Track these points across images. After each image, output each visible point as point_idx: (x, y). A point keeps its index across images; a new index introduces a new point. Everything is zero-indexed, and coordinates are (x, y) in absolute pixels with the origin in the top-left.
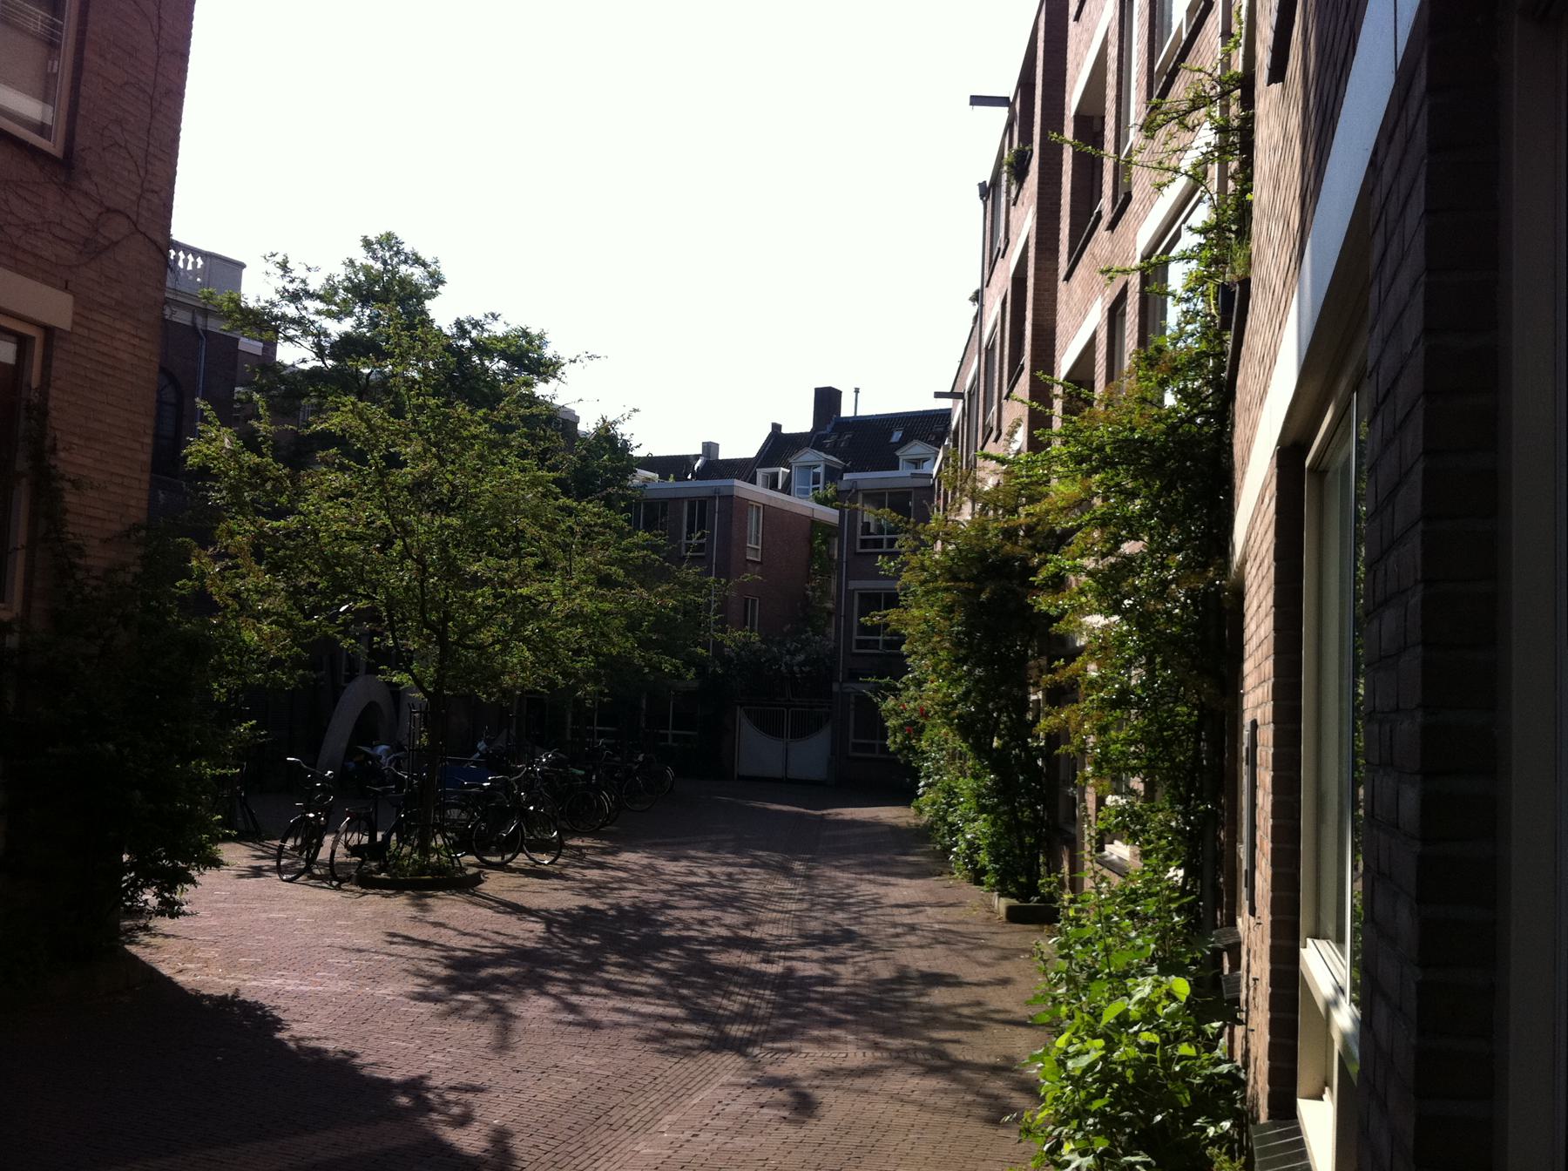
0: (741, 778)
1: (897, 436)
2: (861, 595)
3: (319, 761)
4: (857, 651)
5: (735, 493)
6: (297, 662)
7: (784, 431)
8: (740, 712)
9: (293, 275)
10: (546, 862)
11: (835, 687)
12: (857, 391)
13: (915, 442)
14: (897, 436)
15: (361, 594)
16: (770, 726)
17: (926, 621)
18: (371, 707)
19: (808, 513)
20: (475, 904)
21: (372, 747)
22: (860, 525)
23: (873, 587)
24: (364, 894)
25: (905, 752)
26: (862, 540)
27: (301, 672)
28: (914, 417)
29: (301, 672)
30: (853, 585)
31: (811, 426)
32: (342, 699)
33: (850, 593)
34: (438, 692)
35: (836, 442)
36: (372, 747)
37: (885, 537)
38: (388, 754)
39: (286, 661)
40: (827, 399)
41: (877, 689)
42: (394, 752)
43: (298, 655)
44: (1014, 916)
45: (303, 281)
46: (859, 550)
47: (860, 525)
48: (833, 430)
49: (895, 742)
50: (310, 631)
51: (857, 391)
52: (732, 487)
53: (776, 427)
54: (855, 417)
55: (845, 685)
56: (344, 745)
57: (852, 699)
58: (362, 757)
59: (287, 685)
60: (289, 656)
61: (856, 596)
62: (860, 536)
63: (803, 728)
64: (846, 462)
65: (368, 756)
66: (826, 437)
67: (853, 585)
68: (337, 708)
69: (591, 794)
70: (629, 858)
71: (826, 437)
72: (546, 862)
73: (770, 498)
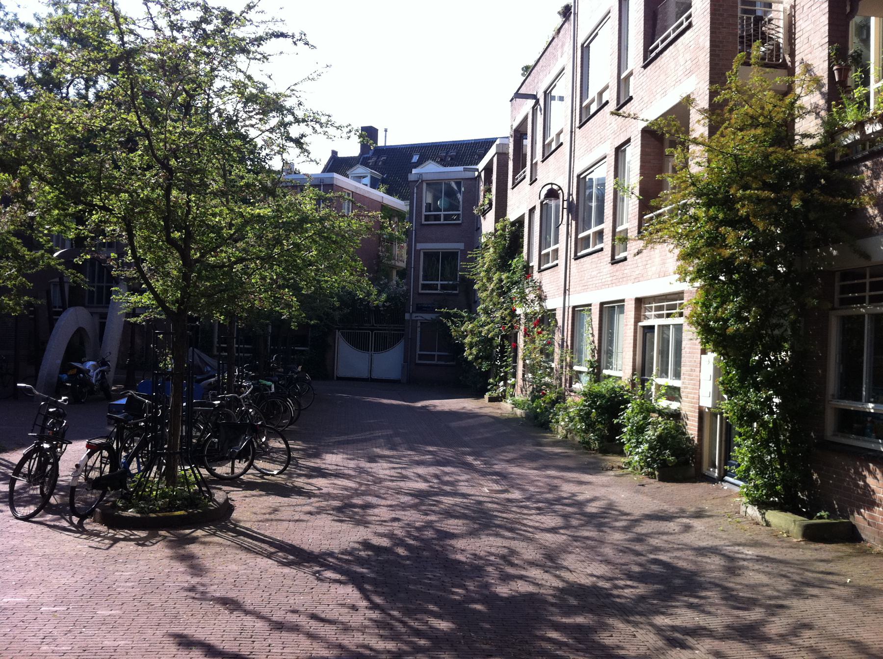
0: (340, 379)
1: (415, 158)
2: (425, 253)
3: (40, 375)
4: (423, 292)
5: (335, 183)
6: (21, 290)
7: (339, 155)
8: (338, 334)
9: (6, 10)
10: (275, 472)
11: (407, 316)
12: (386, 131)
13: (430, 161)
14: (415, 158)
15: (96, 205)
16: (360, 343)
17: (707, 232)
18: (80, 332)
19: (380, 200)
20: (248, 550)
21: (82, 363)
22: (424, 205)
23: (441, 247)
24: (115, 541)
25: (480, 361)
26: (425, 215)
27: (26, 298)
28: (429, 147)
29: (26, 298)
30: (420, 246)
31: (359, 151)
32: (56, 325)
33: (418, 252)
34: (181, 312)
35: (376, 162)
36: (82, 363)
37: (442, 213)
38: (95, 368)
39: (12, 289)
40: (369, 133)
41: (448, 316)
42: (100, 367)
43: (22, 284)
44: (812, 535)
45: (15, 15)
46: (424, 222)
47: (424, 205)
48: (374, 154)
49: (471, 354)
50: (34, 262)
51: (386, 131)
52: (333, 178)
53: (334, 153)
54: (385, 146)
55: (414, 315)
56: (59, 361)
57: (419, 324)
58: (76, 370)
59: (15, 311)
60: (14, 285)
61: (422, 254)
62: (424, 213)
63: (383, 345)
64: (383, 174)
65: (80, 371)
66: (369, 158)
67: (420, 246)
68: (53, 332)
69: (278, 401)
70: (332, 460)
71: (369, 158)
72: (275, 472)
73: (357, 188)
